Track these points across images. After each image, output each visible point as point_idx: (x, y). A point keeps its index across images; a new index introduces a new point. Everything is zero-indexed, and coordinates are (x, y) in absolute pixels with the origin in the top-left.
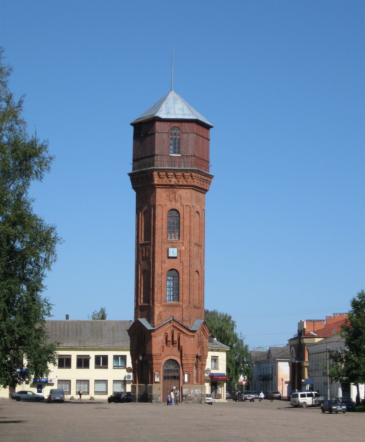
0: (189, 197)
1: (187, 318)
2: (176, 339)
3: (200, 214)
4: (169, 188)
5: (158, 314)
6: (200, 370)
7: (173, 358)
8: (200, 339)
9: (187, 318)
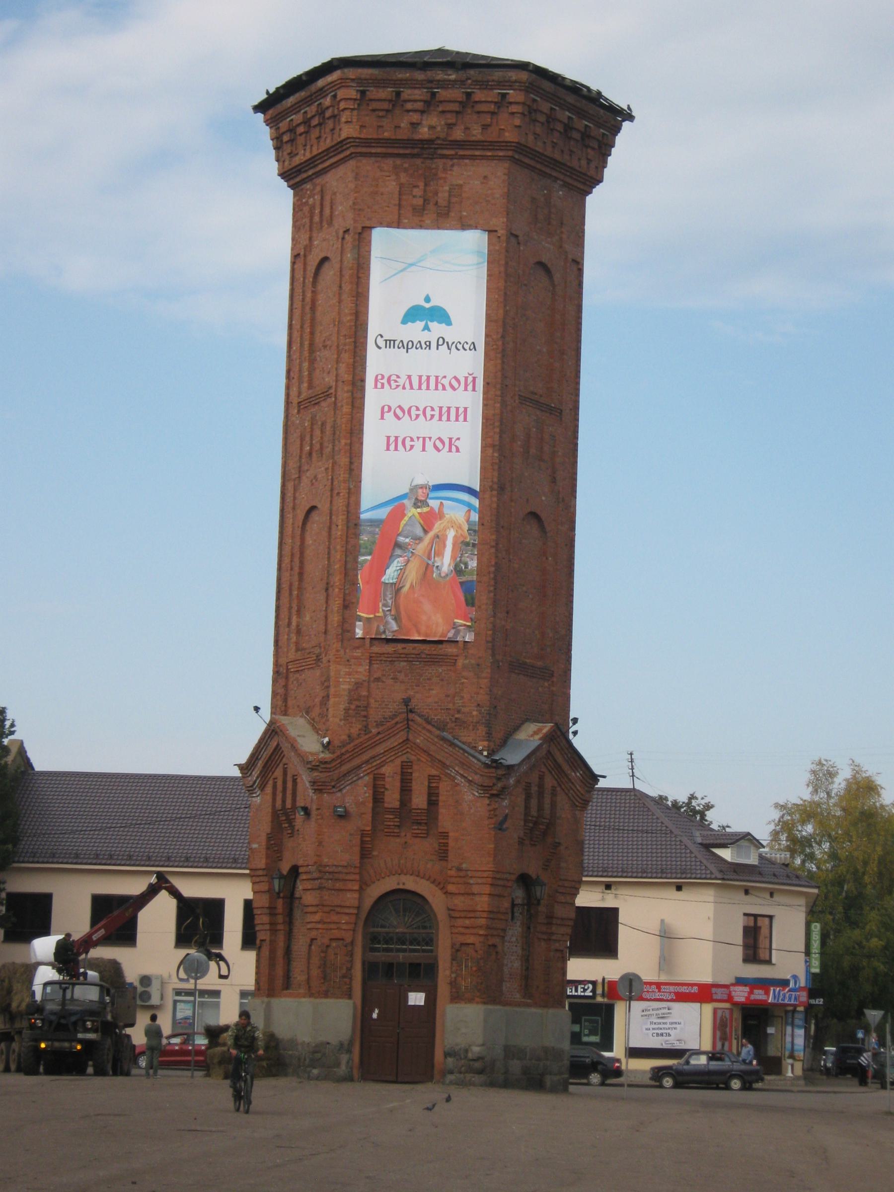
0: (497, 196)
1: (475, 713)
2: (419, 800)
3: (557, 276)
4: (413, 156)
5: (350, 691)
6: (543, 944)
7: (410, 883)
8: (540, 808)
9: (475, 713)
